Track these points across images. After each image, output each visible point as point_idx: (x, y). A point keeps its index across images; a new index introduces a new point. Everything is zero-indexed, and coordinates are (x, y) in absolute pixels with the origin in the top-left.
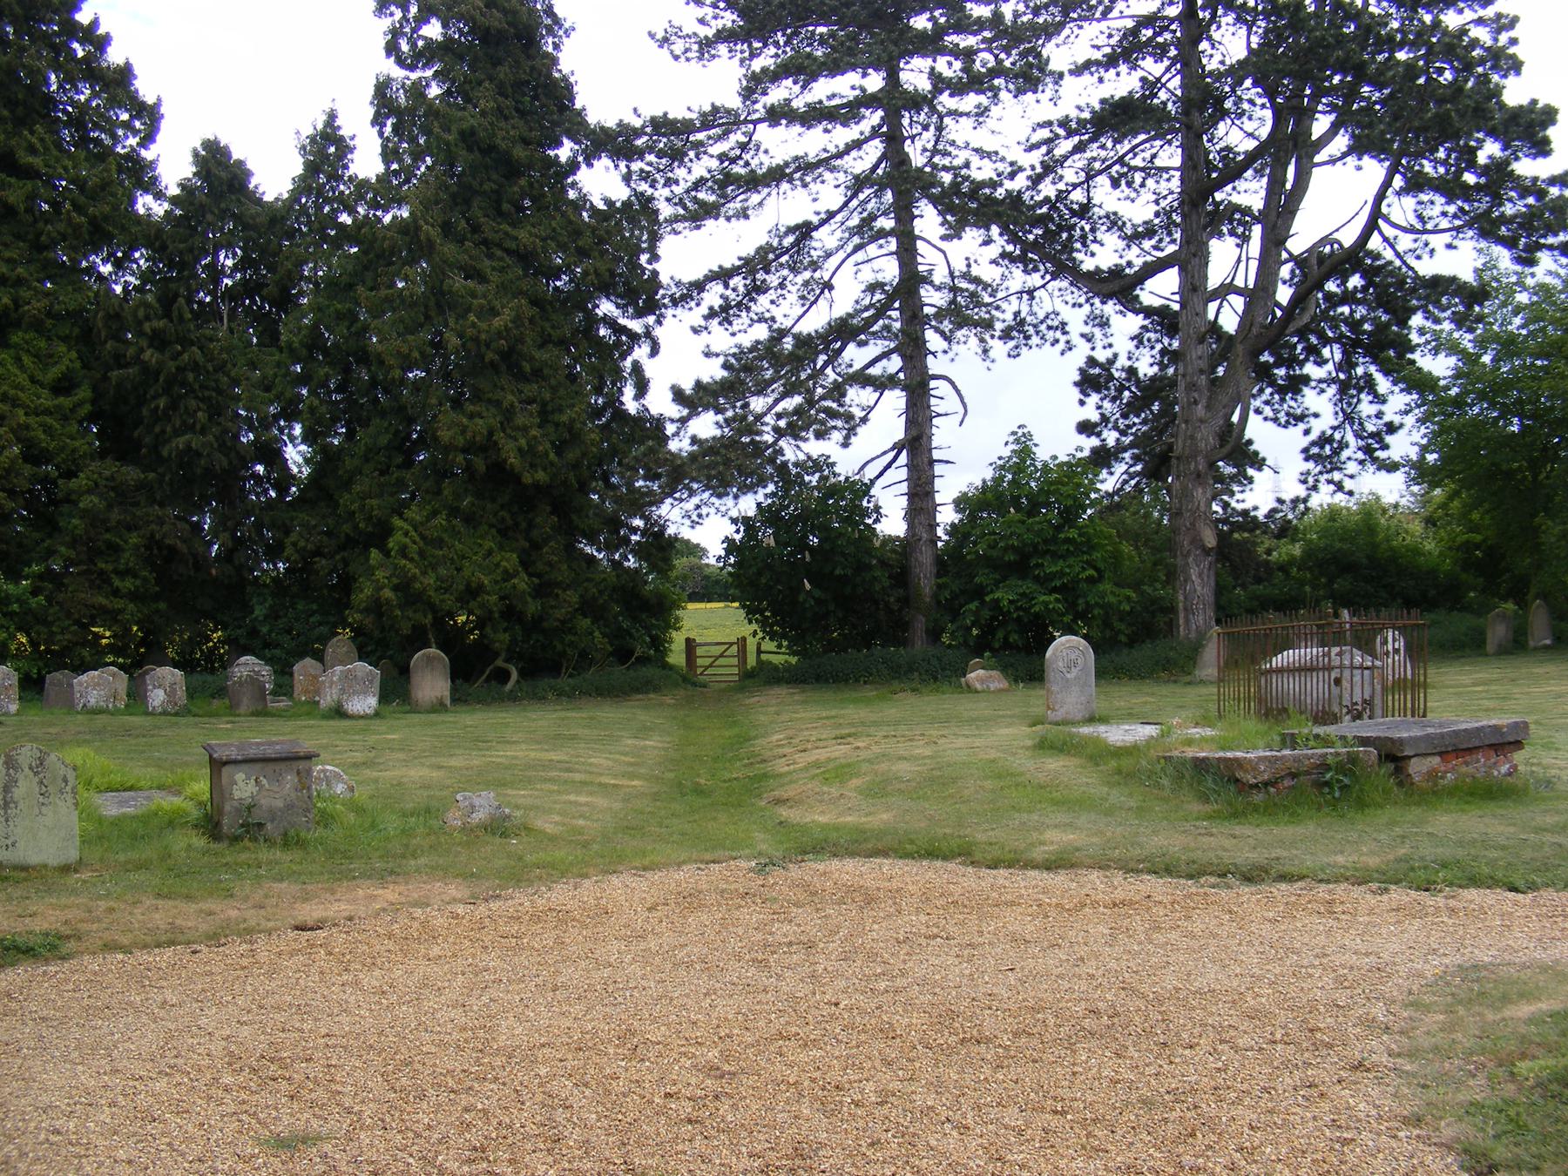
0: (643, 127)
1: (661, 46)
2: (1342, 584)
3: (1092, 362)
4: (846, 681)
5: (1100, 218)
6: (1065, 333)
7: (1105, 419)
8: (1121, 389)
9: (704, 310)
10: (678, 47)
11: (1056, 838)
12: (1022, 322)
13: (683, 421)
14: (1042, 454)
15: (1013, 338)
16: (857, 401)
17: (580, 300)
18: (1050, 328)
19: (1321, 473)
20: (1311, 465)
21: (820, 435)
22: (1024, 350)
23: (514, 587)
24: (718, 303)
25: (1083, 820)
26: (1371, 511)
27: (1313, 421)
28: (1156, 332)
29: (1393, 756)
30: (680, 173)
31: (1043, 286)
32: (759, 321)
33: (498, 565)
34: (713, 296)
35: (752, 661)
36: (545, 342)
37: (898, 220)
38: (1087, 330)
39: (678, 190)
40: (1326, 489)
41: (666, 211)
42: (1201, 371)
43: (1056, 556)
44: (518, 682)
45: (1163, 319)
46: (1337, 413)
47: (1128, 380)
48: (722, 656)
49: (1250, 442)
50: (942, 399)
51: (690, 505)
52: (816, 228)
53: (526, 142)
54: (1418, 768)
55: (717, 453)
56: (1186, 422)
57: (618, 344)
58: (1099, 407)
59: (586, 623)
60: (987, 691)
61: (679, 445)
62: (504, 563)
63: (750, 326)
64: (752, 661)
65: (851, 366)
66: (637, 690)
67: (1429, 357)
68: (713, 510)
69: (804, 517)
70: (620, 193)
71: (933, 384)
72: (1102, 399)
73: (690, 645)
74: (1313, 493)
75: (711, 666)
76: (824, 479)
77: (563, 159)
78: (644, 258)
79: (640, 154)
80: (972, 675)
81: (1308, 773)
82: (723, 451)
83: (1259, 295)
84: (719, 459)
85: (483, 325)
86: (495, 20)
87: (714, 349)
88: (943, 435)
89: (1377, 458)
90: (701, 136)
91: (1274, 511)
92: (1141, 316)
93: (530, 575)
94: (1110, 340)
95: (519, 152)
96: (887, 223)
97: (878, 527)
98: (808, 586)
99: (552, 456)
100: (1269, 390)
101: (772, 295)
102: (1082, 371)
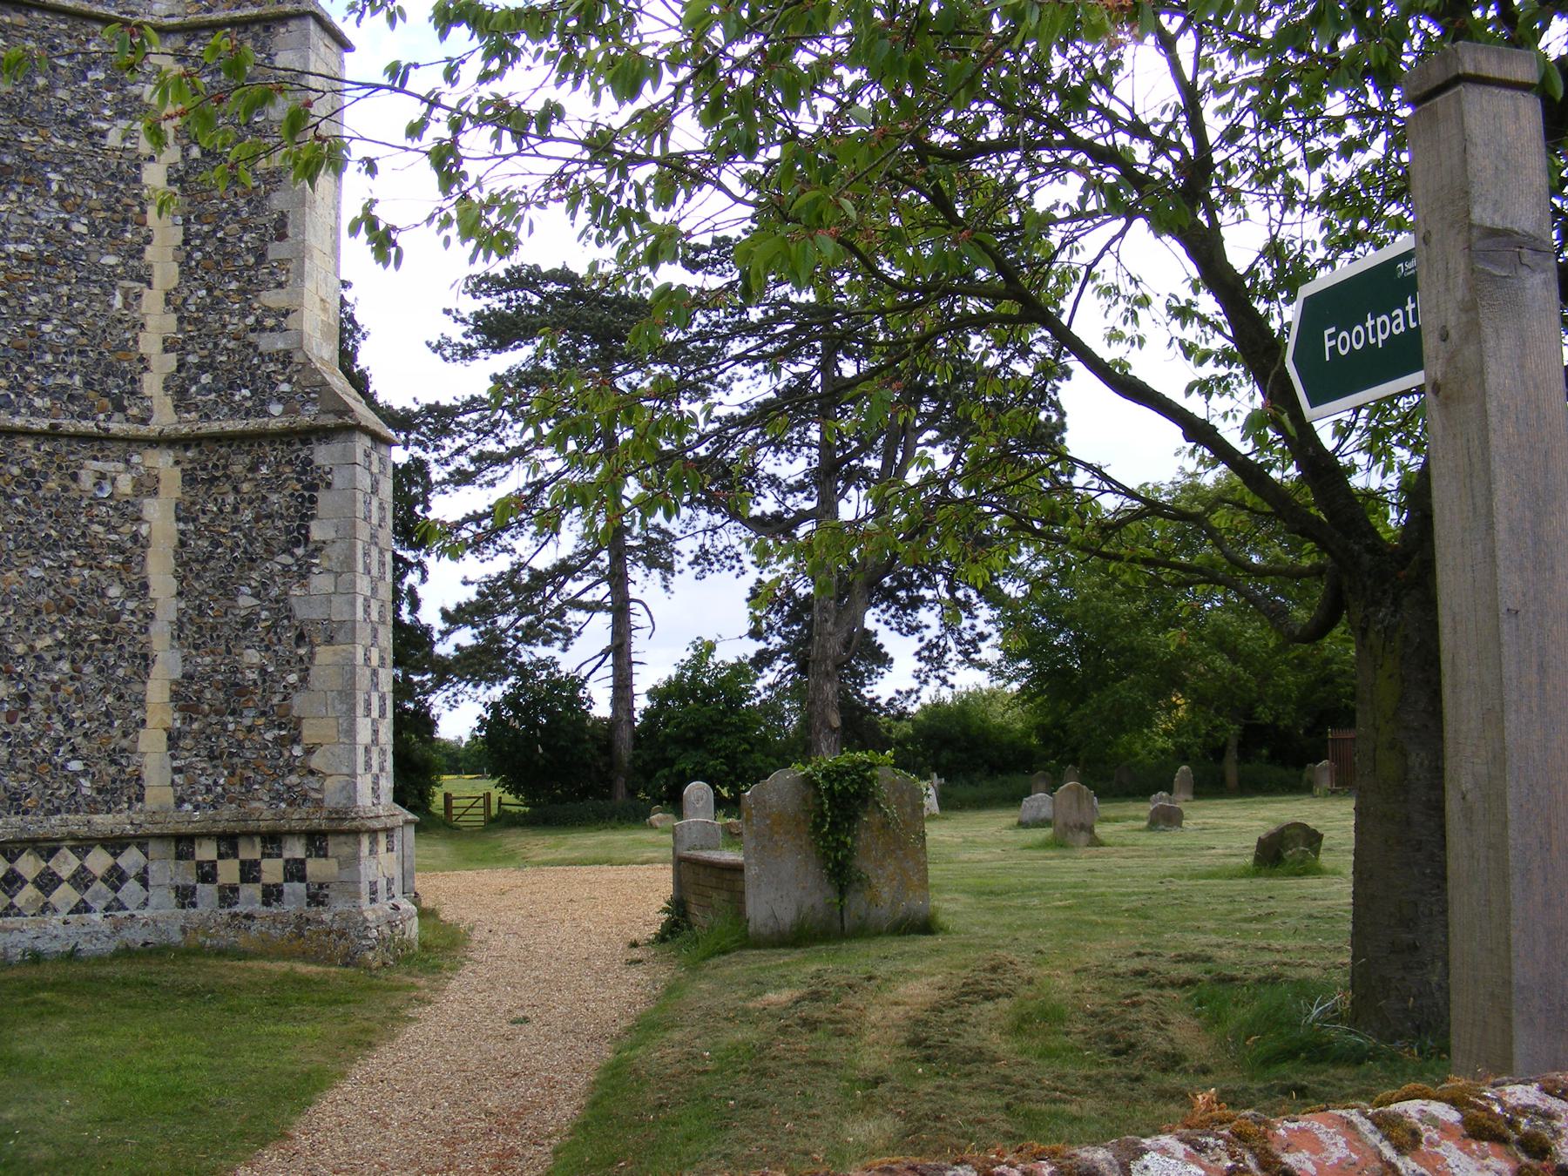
2: (946, 756)
8: (782, 604)
10: (448, 353)
13: (445, 634)
20: (922, 664)
21: (547, 643)
22: (708, 574)
30: (447, 442)
35: (494, 811)
40: (934, 683)
41: (437, 473)
43: (721, 733)
49: (881, 646)
50: (638, 618)
51: (450, 693)
71: (632, 605)
73: (448, 798)
76: (550, 675)
78: (418, 509)
79: (417, 428)
87: (470, 579)
91: (893, 699)
101: (513, 532)
102: (752, 590)
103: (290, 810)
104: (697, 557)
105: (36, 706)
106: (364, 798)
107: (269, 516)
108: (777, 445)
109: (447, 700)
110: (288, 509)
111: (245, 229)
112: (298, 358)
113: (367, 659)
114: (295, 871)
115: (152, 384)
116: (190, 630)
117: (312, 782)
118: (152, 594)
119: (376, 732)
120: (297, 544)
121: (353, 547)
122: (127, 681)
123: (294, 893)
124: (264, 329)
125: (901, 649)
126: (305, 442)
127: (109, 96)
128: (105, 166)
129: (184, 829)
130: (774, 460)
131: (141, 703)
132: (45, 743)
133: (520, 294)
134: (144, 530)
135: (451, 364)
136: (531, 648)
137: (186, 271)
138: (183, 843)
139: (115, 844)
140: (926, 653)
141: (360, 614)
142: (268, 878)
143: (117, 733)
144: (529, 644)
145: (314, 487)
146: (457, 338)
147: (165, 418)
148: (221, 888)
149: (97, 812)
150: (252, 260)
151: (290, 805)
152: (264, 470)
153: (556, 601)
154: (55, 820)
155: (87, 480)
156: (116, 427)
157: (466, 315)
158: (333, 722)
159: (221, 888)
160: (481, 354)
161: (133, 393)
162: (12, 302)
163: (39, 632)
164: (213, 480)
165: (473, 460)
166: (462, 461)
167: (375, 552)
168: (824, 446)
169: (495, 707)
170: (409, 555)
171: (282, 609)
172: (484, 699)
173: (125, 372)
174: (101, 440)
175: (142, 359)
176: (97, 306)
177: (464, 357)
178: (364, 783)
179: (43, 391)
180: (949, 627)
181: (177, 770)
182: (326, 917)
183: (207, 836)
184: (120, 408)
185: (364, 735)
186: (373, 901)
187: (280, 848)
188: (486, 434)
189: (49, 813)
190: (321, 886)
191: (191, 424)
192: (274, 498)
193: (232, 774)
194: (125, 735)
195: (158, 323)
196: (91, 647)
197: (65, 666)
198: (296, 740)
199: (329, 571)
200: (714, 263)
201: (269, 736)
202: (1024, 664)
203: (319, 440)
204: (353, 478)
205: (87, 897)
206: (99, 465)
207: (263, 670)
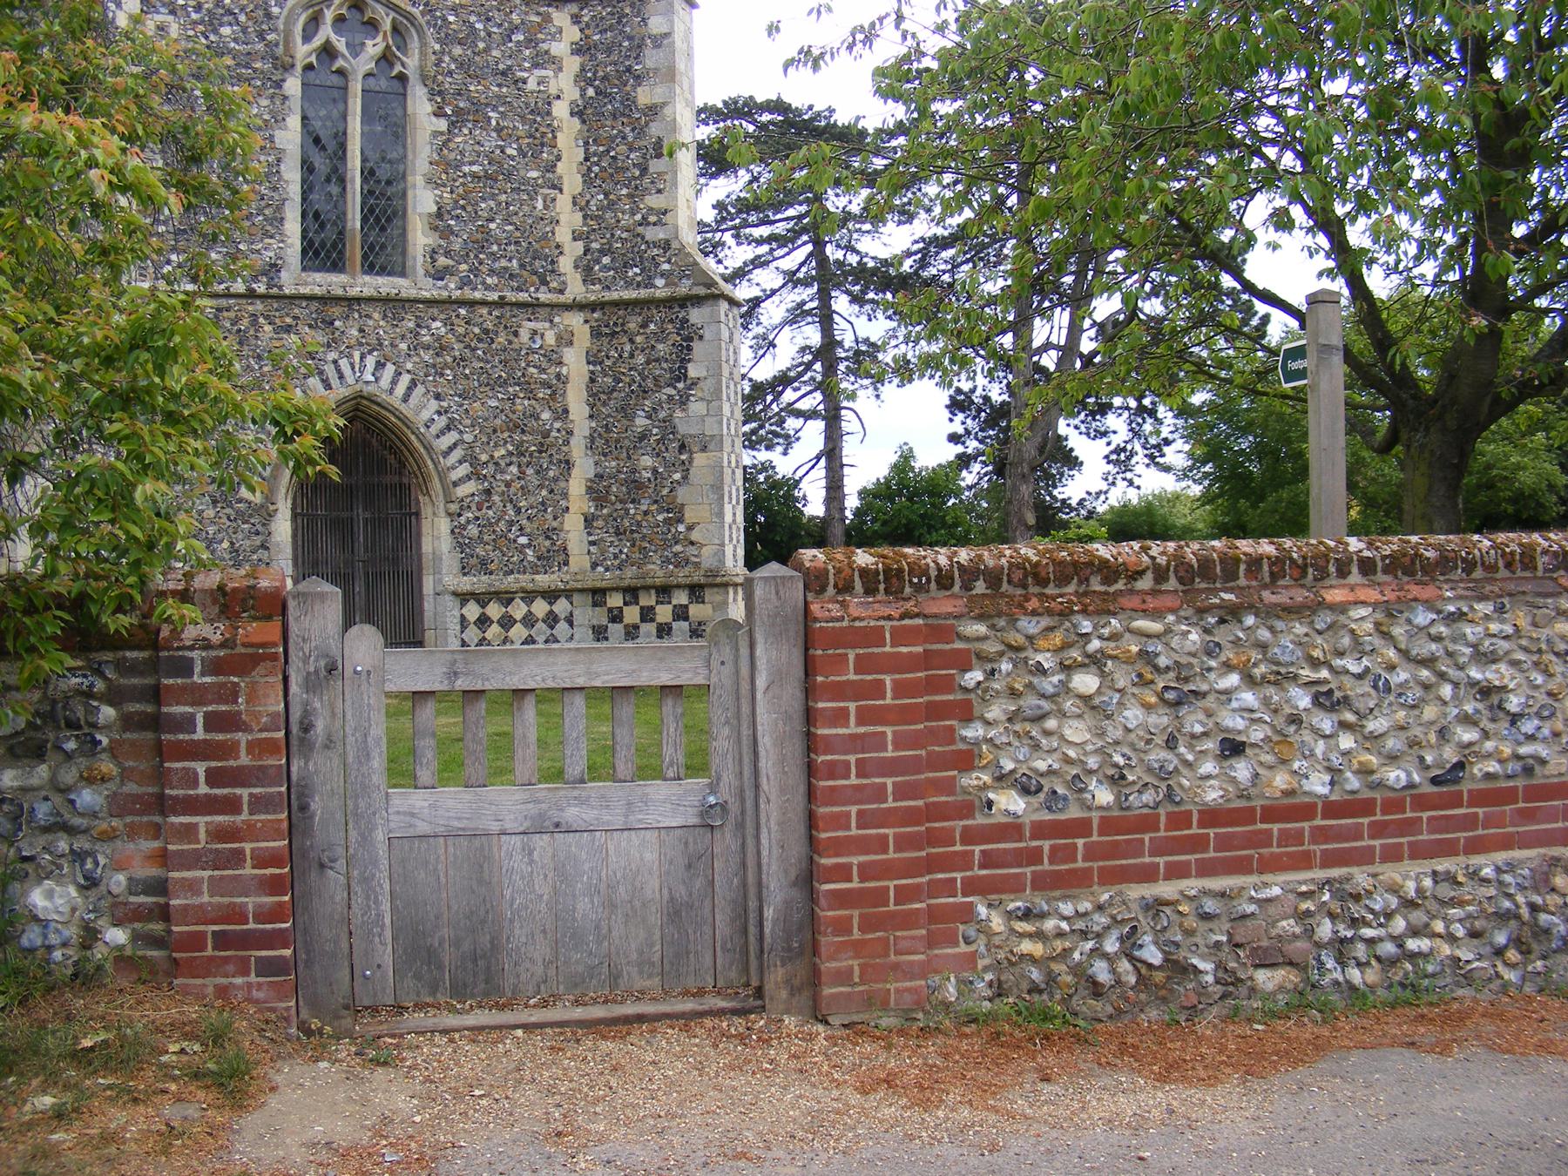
7: (968, 432)
8: (980, 410)
14: (917, 465)
20: (1111, 467)
21: (768, 448)
40: (1121, 485)
49: (1072, 450)
50: (849, 423)
71: (843, 412)
83: (1069, 349)
88: (850, 449)
91: (1083, 500)
105: (496, 498)
106: (729, 563)
107: (657, 360)
111: (631, 149)
112: (675, 245)
114: (681, 614)
115: (565, 264)
116: (599, 442)
117: (692, 550)
118: (571, 417)
122: (556, 480)
123: (680, 629)
124: (648, 224)
125: (1090, 452)
126: (683, 306)
127: (527, 52)
128: (527, 104)
129: (598, 585)
131: (565, 495)
132: (502, 525)
134: (564, 371)
137: (588, 180)
138: (597, 595)
139: (551, 595)
140: (1114, 457)
142: (660, 619)
143: (550, 517)
145: (691, 339)
147: (576, 289)
148: (626, 626)
149: (538, 573)
150: (637, 173)
152: (652, 326)
154: (511, 578)
155: (524, 336)
156: (544, 296)
159: (626, 626)
161: (553, 271)
162: (469, 208)
163: (496, 445)
164: (614, 334)
171: (668, 426)
173: (547, 256)
174: (533, 307)
175: (558, 246)
176: (526, 208)
178: (729, 550)
179: (492, 272)
181: (592, 543)
183: (616, 589)
184: (545, 283)
185: (728, 518)
189: (507, 574)
190: (699, 624)
191: (595, 293)
192: (660, 347)
193: (633, 545)
194: (555, 518)
195: (568, 220)
196: (531, 455)
197: (514, 469)
198: (680, 520)
201: (660, 518)
202: (1208, 468)
205: (533, 632)
206: (532, 325)
207: (655, 471)
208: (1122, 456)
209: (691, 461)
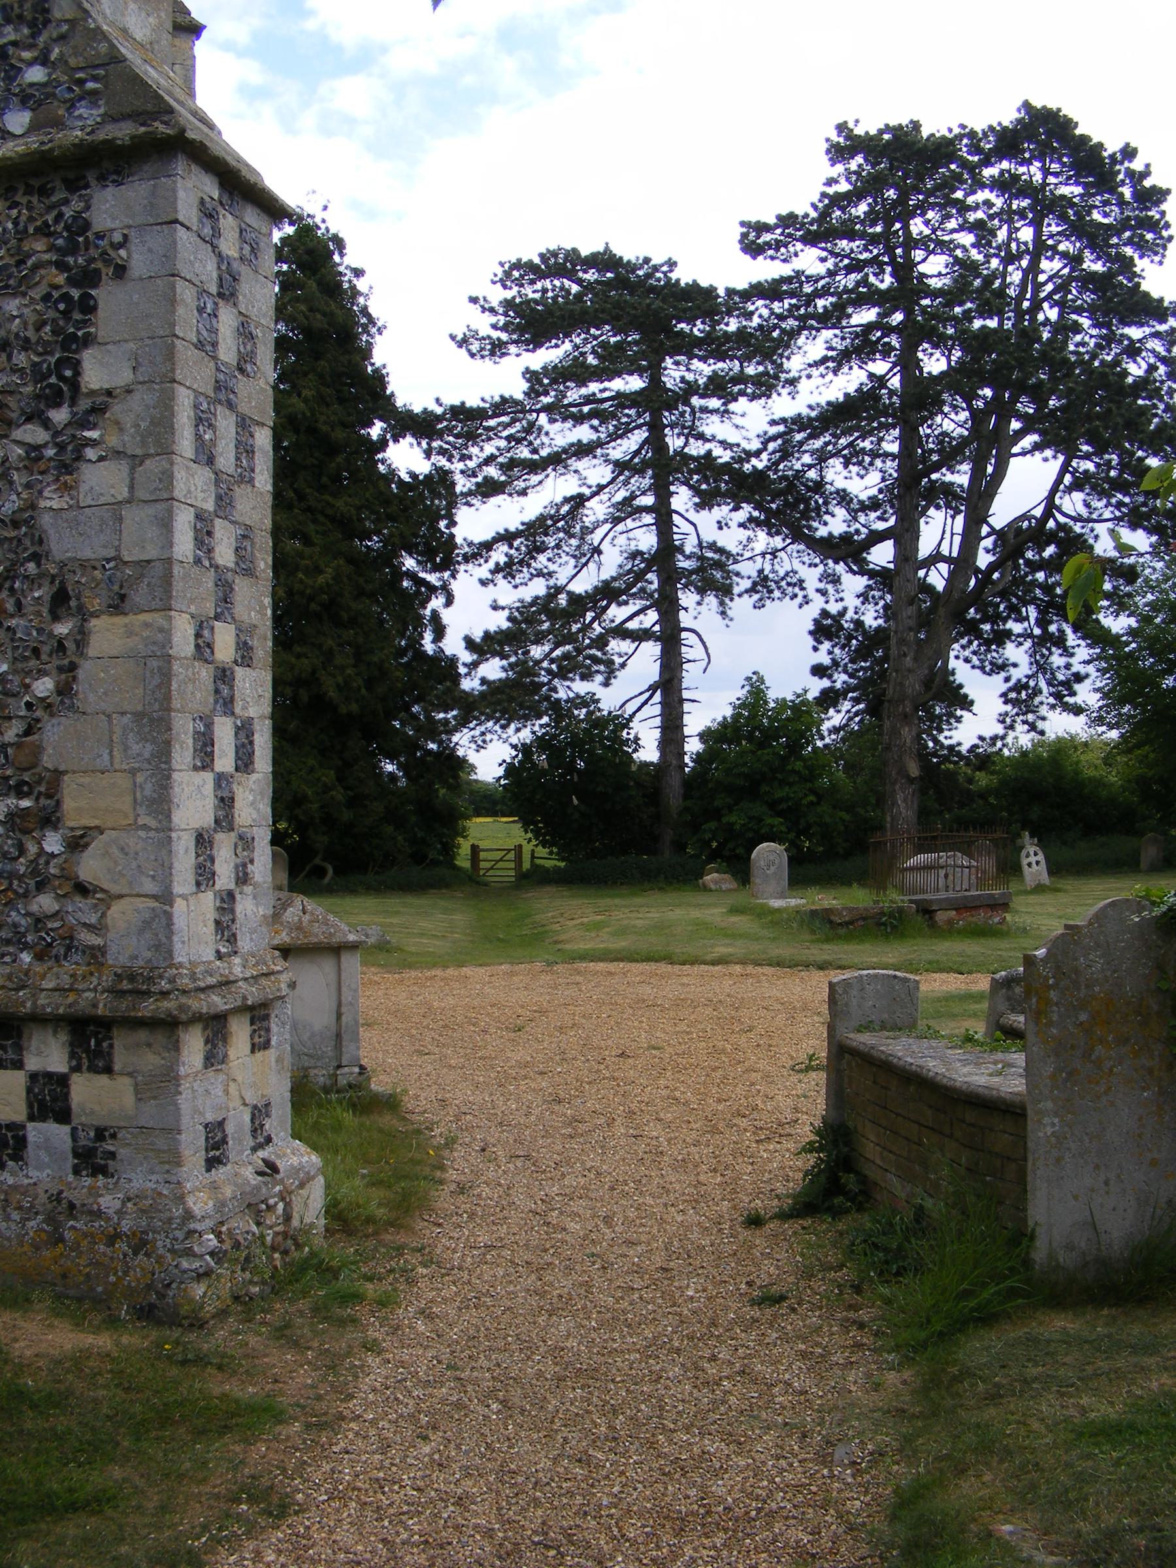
0: (444, 414)
1: (460, 346)
2: (1035, 813)
3: (825, 613)
4: (606, 882)
5: (831, 494)
6: (803, 589)
7: (835, 663)
8: (850, 638)
9: (491, 565)
10: (475, 347)
11: (721, 950)
12: (766, 578)
13: (474, 665)
15: (757, 592)
16: (617, 650)
17: (389, 558)
18: (789, 584)
19: (1017, 714)
20: (1009, 708)
21: (586, 677)
22: (768, 602)
23: (333, 798)
24: (503, 560)
25: (739, 943)
26: (1064, 747)
27: (1012, 670)
28: (879, 590)
29: (926, 911)
30: (474, 450)
31: (783, 549)
32: (538, 575)
33: (318, 779)
34: (499, 555)
35: (526, 865)
36: (361, 593)
37: (657, 496)
38: (821, 586)
39: (471, 464)
40: (1020, 728)
41: (462, 484)
42: (910, 629)
44: (332, 878)
45: (882, 578)
46: (1031, 664)
47: (856, 630)
48: (492, 868)
49: (961, 686)
50: (691, 650)
51: (477, 732)
52: (588, 499)
53: (344, 425)
54: (941, 917)
55: (503, 692)
56: (897, 671)
57: (418, 592)
58: (830, 653)
59: (389, 829)
60: (720, 890)
61: (469, 684)
62: (324, 778)
63: (530, 580)
64: (526, 865)
65: (613, 621)
66: (432, 886)
67: (1111, 618)
68: (495, 737)
69: (576, 743)
70: (423, 467)
71: (684, 635)
72: (833, 647)
73: (475, 849)
74: (1010, 732)
75: (492, 868)
76: (590, 713)
77: (375, 438)
78: (442, 524)
79: (440, 435)
80: (708, 877)
81: (872, 918)
82: (507, 690)
83: (962, 563)
84: (504, 697)
85: (310, 582)
86: (319, 322)
87: (501, 603)
88: (691, 675)
89: (1067, 703)
90: (492, 423)
91: (975, 746)
92: (866, 577)
93: (345, 788)
94: (841, 595)
95: (339, 435)
96: (648, 500)
97: (635, 756)
98: (575, 802)
99: (364, 691)
100: (976, 643)
103: (39, 968)
104: (755, 584)
108: (852, 457)
109: (473, 740)
110: (39, 327)
113: (203, 648)
117: (82, 910)
119: (226, 803)
120: (55, 399)
121: (167, 404)
130: (845, 473)
133: (557, 283)
135: (478, 362)
136: (568, 683)
140: (1013, 695)
141: (184, 545)
144: (565, 678)
146: (485, 330)
151: (39, 957)
153: (597, 629)
157: (495, 303)
158: (123, 781)
160: (513, 349)
165: (502, 466)
166: (492, 471)
167: (226, 423)
168: (905, 456)
169: (525, 749)
170: (432, 578)
172: (514, 740)
177: (493, 354)
180: (1041, 667)
182: (109, 1202)
186: (212, 1163)
187: (19, 1049)
188: (519, 441)
198: (49, 820)
199: (118, 454)
200: (778, 245)
203: (102, 179)
204: (170, 253)
208: (1023, 695)
209: (82, 638)
